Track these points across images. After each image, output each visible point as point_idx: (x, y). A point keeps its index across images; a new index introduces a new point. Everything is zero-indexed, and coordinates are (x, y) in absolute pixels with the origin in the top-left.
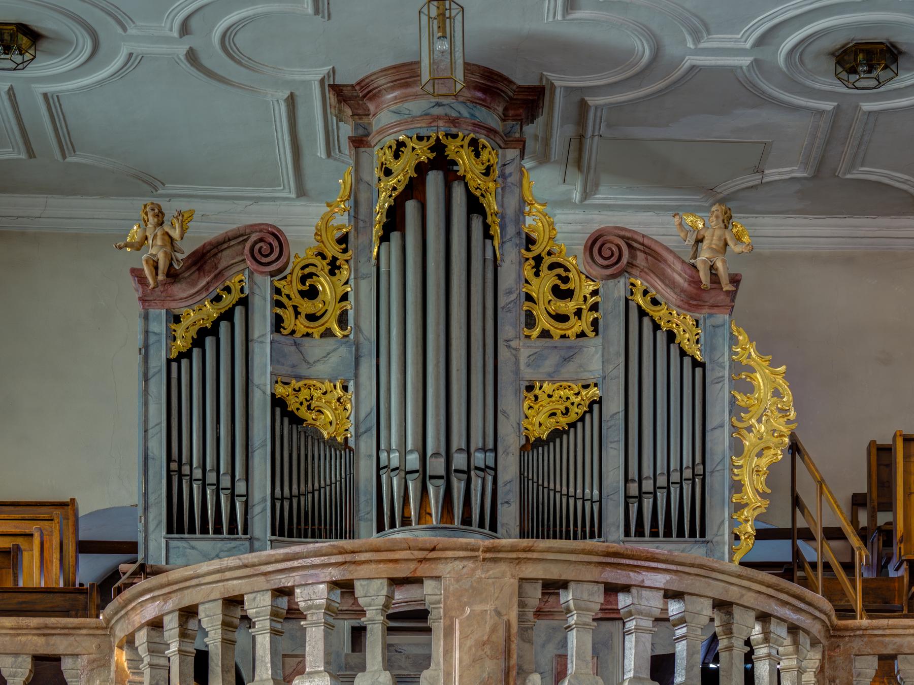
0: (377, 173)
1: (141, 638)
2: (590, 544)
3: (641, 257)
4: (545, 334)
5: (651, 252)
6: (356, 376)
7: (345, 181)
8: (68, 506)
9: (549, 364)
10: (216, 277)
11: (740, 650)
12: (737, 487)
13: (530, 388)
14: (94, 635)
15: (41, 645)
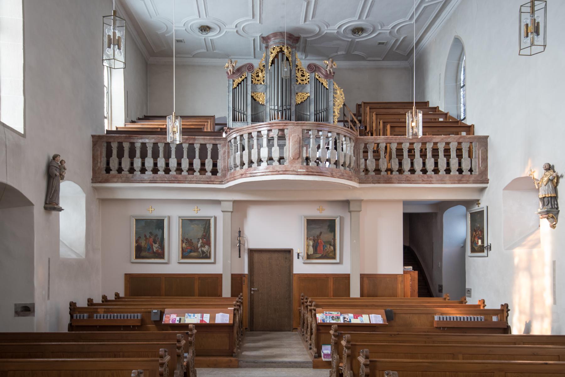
0: (270, 53)
1: (233, 141)
2: (309, 122)
3: (317, 69)
4: (300, 83)
5: (318, 68)
6: (266, 92)
7: (264, 55)
8: (214, 117)
9: (300, 89)
10: (241, 73)
11: (341, 143)
12: (334, 112)
13: (297, 94)
14: (224, 140)
15: (214, 142)
